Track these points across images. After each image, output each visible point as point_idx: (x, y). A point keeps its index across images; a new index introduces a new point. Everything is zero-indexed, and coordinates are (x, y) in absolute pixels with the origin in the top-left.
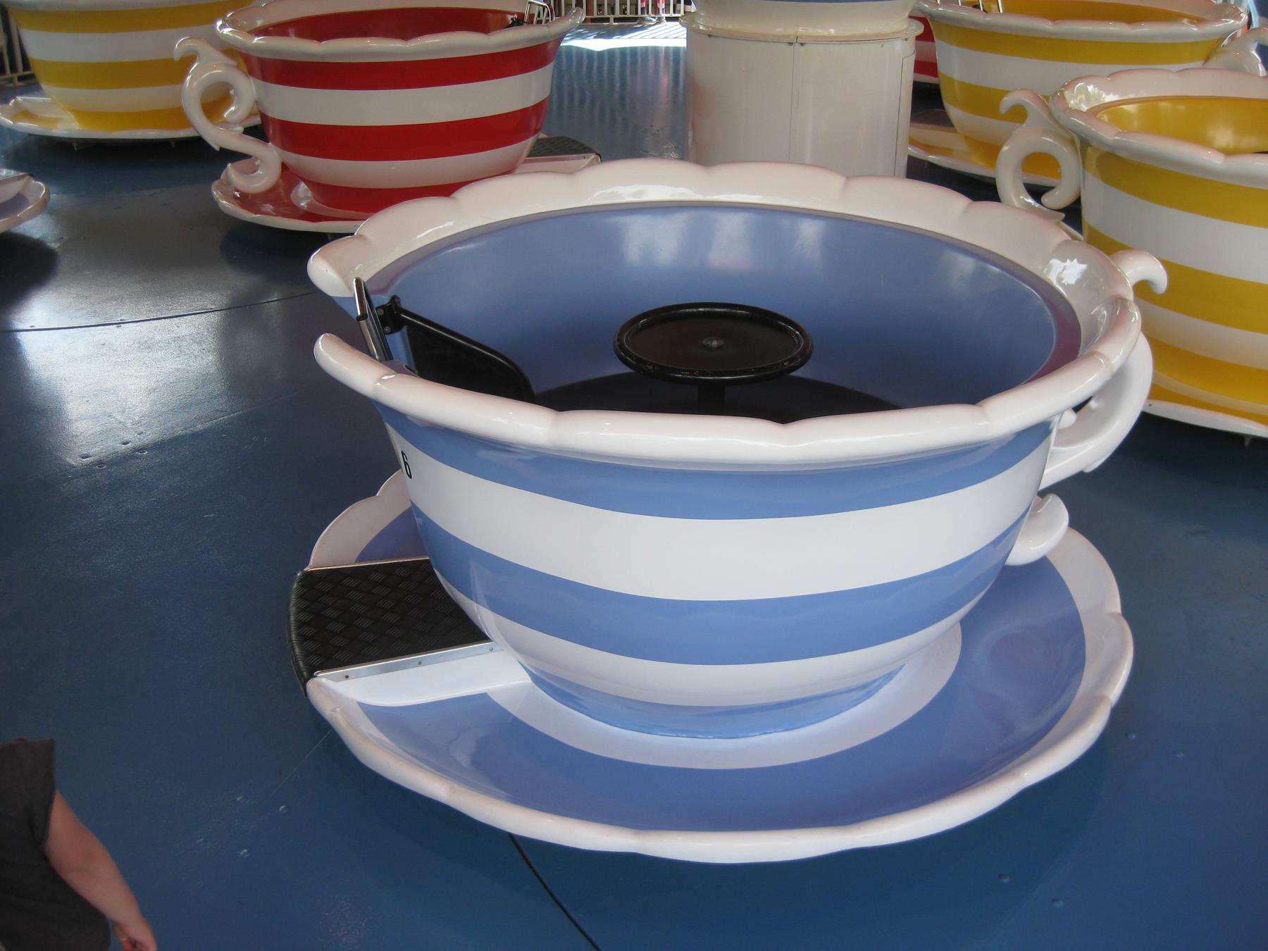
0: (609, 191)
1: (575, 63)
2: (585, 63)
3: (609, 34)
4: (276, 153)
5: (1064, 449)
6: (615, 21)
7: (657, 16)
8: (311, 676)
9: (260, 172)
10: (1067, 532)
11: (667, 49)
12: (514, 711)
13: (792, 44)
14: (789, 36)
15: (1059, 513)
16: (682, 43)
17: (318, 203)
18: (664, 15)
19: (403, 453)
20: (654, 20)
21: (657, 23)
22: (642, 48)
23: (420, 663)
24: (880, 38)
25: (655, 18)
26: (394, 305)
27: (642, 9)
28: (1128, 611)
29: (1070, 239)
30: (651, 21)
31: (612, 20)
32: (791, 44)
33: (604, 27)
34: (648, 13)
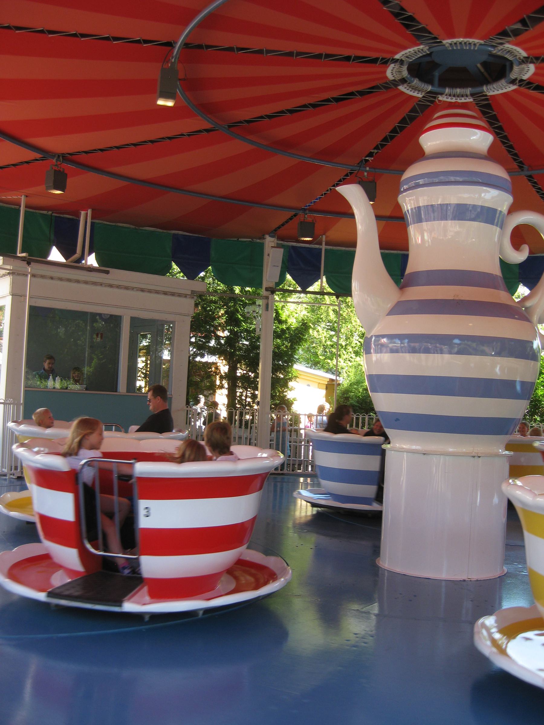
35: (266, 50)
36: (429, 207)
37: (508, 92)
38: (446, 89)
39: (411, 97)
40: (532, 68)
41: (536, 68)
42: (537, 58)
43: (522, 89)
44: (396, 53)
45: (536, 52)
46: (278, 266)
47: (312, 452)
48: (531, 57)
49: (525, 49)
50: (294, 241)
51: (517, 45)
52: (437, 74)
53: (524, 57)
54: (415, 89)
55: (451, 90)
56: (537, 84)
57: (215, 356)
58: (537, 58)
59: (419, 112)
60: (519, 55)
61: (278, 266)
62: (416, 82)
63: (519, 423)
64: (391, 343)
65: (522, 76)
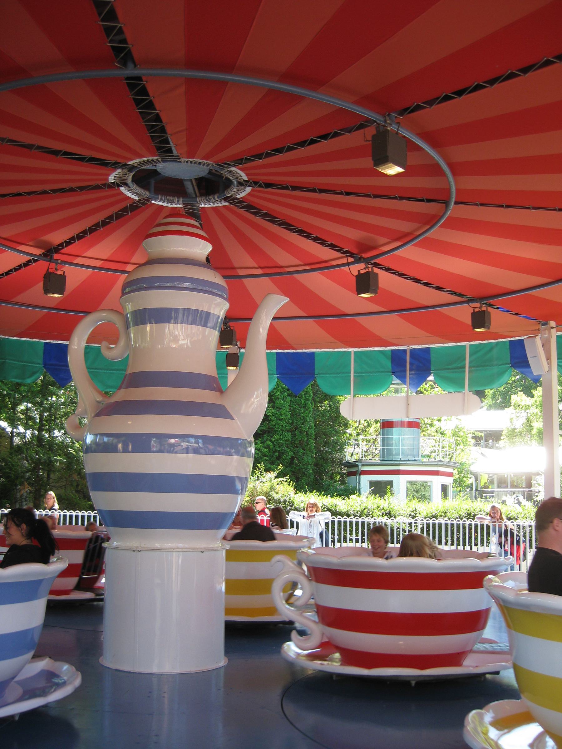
36: (196, 310)
39: (129, 198)
40: (111, 179)
41: (107, 179)
42: (256, 183)
44: (131, 160)
45: (257, 178)
47: (58, 595)
48: (251, 181)
49: (247, 175)
51: (242, 170)
52: (153, 182)
53: (244, 181)
54: (133, 192)
55: (165, 197)
57: (102, 641)
58: (256, 183)
62: (134, 187)
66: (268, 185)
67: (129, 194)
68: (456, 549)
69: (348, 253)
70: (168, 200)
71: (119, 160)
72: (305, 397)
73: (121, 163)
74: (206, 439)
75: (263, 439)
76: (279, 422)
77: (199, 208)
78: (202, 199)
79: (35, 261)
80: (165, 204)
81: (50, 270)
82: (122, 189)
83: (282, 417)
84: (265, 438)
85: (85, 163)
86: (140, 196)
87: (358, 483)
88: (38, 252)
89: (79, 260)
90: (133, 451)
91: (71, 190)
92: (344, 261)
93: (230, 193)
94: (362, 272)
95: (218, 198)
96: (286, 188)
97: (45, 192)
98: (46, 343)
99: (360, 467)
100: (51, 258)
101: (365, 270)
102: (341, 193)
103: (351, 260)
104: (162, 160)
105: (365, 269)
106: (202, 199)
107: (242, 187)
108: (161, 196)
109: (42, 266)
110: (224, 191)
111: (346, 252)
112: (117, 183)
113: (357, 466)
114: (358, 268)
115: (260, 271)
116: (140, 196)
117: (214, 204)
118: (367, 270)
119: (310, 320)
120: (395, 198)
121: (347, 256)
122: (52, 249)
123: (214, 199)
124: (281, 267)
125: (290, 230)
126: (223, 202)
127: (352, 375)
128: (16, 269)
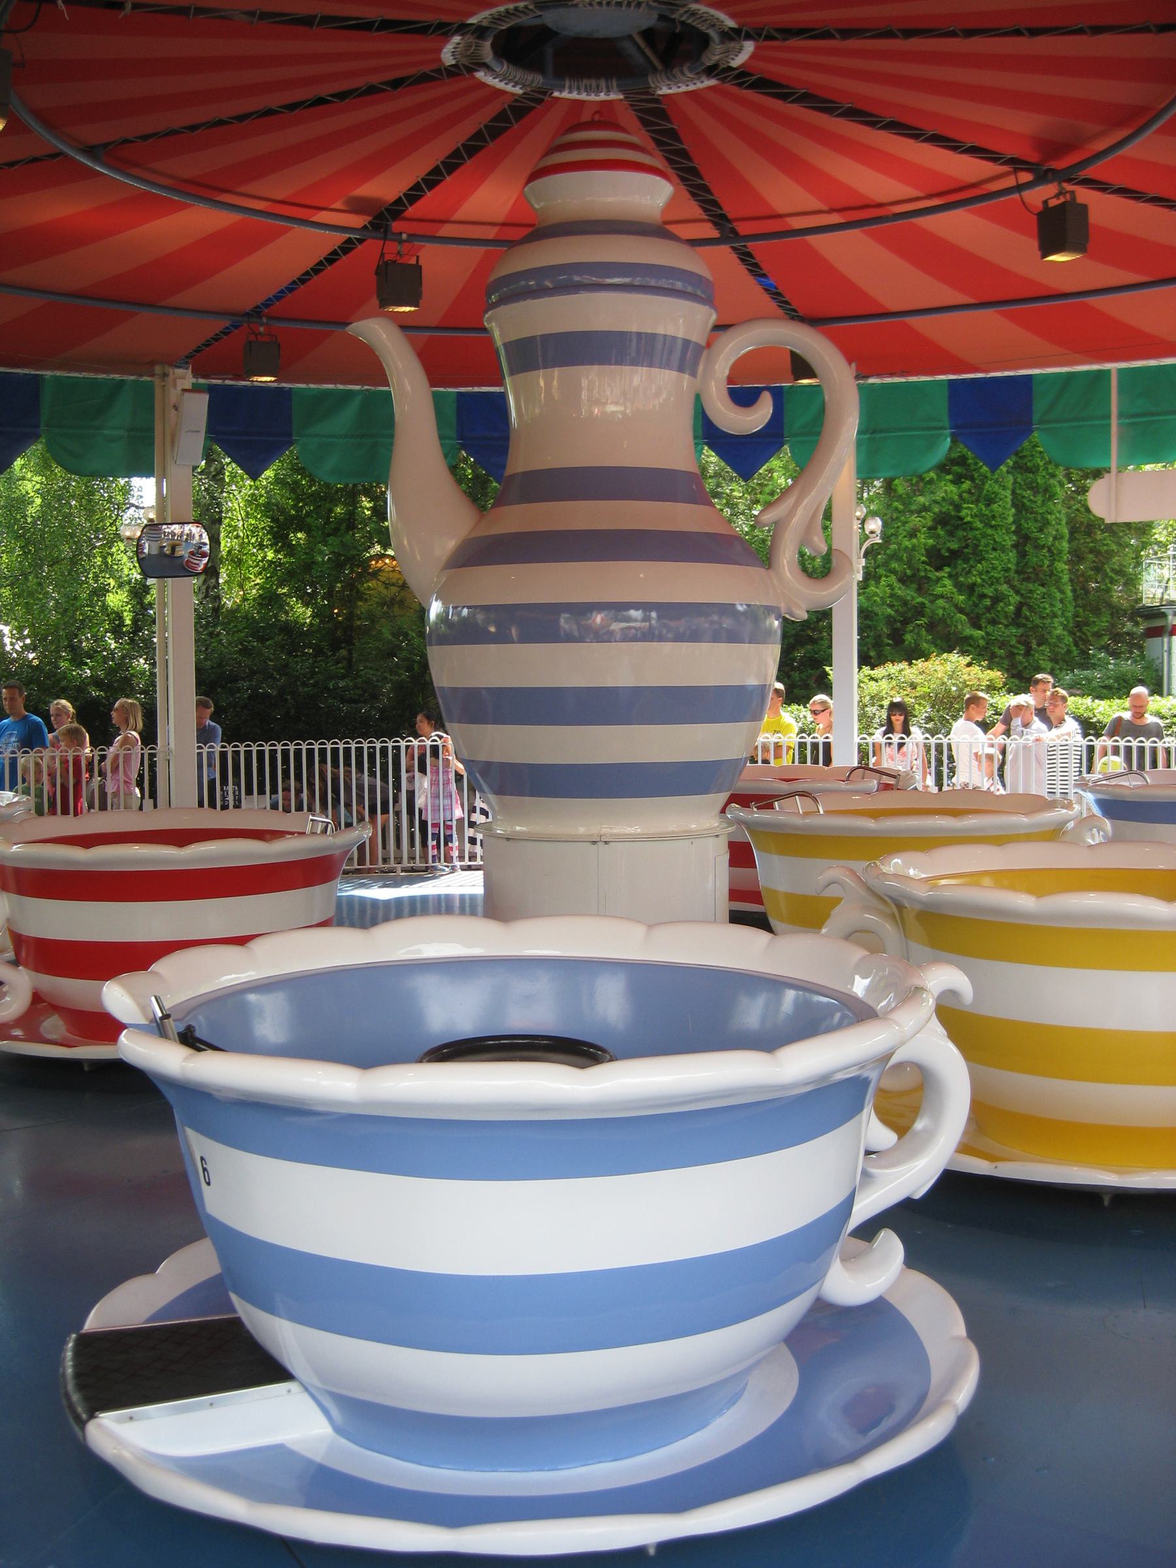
0: (413, 948)
1: (357, 912)
2: (369, 912)
3: (397, 884)
4: (27, 978)
5: (887, 1171)
6: (402, 871)
7: (450, 865)
8: (92, 1416)
9: (8, 999)
10: (902, 1271)
11: (462, 897)
12: (318, 1459)
13: (595, 842)
14: (591, 835)
15: (891, 1246)
16: (479, 890)
17: (69, 1035)
18: (458, 864)
19: (202, 1159)
20: (447, 869)
21: (451, 873)
22: (433, 896)
23: (211, 1404)
24: (689, 836)
25: (448, 867)
26: (189, 1034)
27: (433, 856)
28: (973, 1333)
29: (867, 953)
30: (444, 870)
31: (399, 870)
32: (594, 842)
33: (390, 877)
34: (440, 861)
35: (196, 9)
37: (699, 90)
38: (565, 81)
39: (502, 92)
43: (729, 87)
44: (472, 14)
46: (198, 432)
49: (732, 16)
50: (231, 376)
52: (549, 51)
53: (731, 29)
55: (578, 82)
56: (676, 127)
59: (486, 140)
60: (719, 23)
61: (198, 432)
62: (503, 68)
63: (807, 995)
64: (617, 620)
65: (729, 60)
66: (788, 32)
67: (501, 85)
68: (481, 873)
69: (1017, 164)
70: (586, 86)
71: (445, 18)
72: (1046, 469)
73: (453, 24)
74: (668, 610)
75: (955, 567)
76: (989, 531)
77: (656, 97)
78: (659, 78)
79: (361, 241)
80: (584, 97)
81: (387, 258)
82: (480, 75)
83: (993, 523)
84: (959, 569)
85: (376, 34)
86: (524, 86)
87: (1166, 654)
88: (358, 221)
89: (446, 230)
90: (522, 640)
91: (371, 90)
92: (1010, 182)
93: (714, 56)
94: (1053, 203)
95: (691, 70)
96: (826, 35)
97: (320, 101)
98: (460, 394)
99: (1170, 617)
100: (387, 230)
101: (1058, 199)
102: (953, 34)
103: (1025, 177)
104: (536, 7)
105: (1057, 196)
106: (659, 78)
107: (732, 44)
108: (570, 82)
109: (371, 250)
110: (698, 57)
111: (1012, 161)
112: (462, 64)
113: (1164, 615)
114: (1043, 194)
115: (836, 219)
116: (524, 86)
117: (695, 84)
118: (1062, 200)
119: (989, 312)
120: (1081, 31)
121: (1016, 171)
122: (382, 212)
123: (683, 74)
124: (880, 205)
125: (872, 124)
126: (704, 78)
127: (1114, 422)
128: (318, 269)
